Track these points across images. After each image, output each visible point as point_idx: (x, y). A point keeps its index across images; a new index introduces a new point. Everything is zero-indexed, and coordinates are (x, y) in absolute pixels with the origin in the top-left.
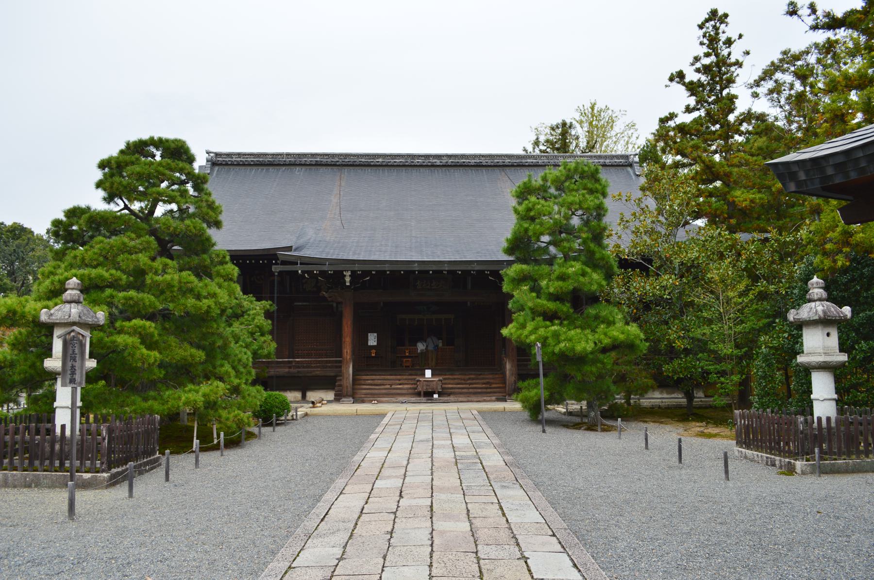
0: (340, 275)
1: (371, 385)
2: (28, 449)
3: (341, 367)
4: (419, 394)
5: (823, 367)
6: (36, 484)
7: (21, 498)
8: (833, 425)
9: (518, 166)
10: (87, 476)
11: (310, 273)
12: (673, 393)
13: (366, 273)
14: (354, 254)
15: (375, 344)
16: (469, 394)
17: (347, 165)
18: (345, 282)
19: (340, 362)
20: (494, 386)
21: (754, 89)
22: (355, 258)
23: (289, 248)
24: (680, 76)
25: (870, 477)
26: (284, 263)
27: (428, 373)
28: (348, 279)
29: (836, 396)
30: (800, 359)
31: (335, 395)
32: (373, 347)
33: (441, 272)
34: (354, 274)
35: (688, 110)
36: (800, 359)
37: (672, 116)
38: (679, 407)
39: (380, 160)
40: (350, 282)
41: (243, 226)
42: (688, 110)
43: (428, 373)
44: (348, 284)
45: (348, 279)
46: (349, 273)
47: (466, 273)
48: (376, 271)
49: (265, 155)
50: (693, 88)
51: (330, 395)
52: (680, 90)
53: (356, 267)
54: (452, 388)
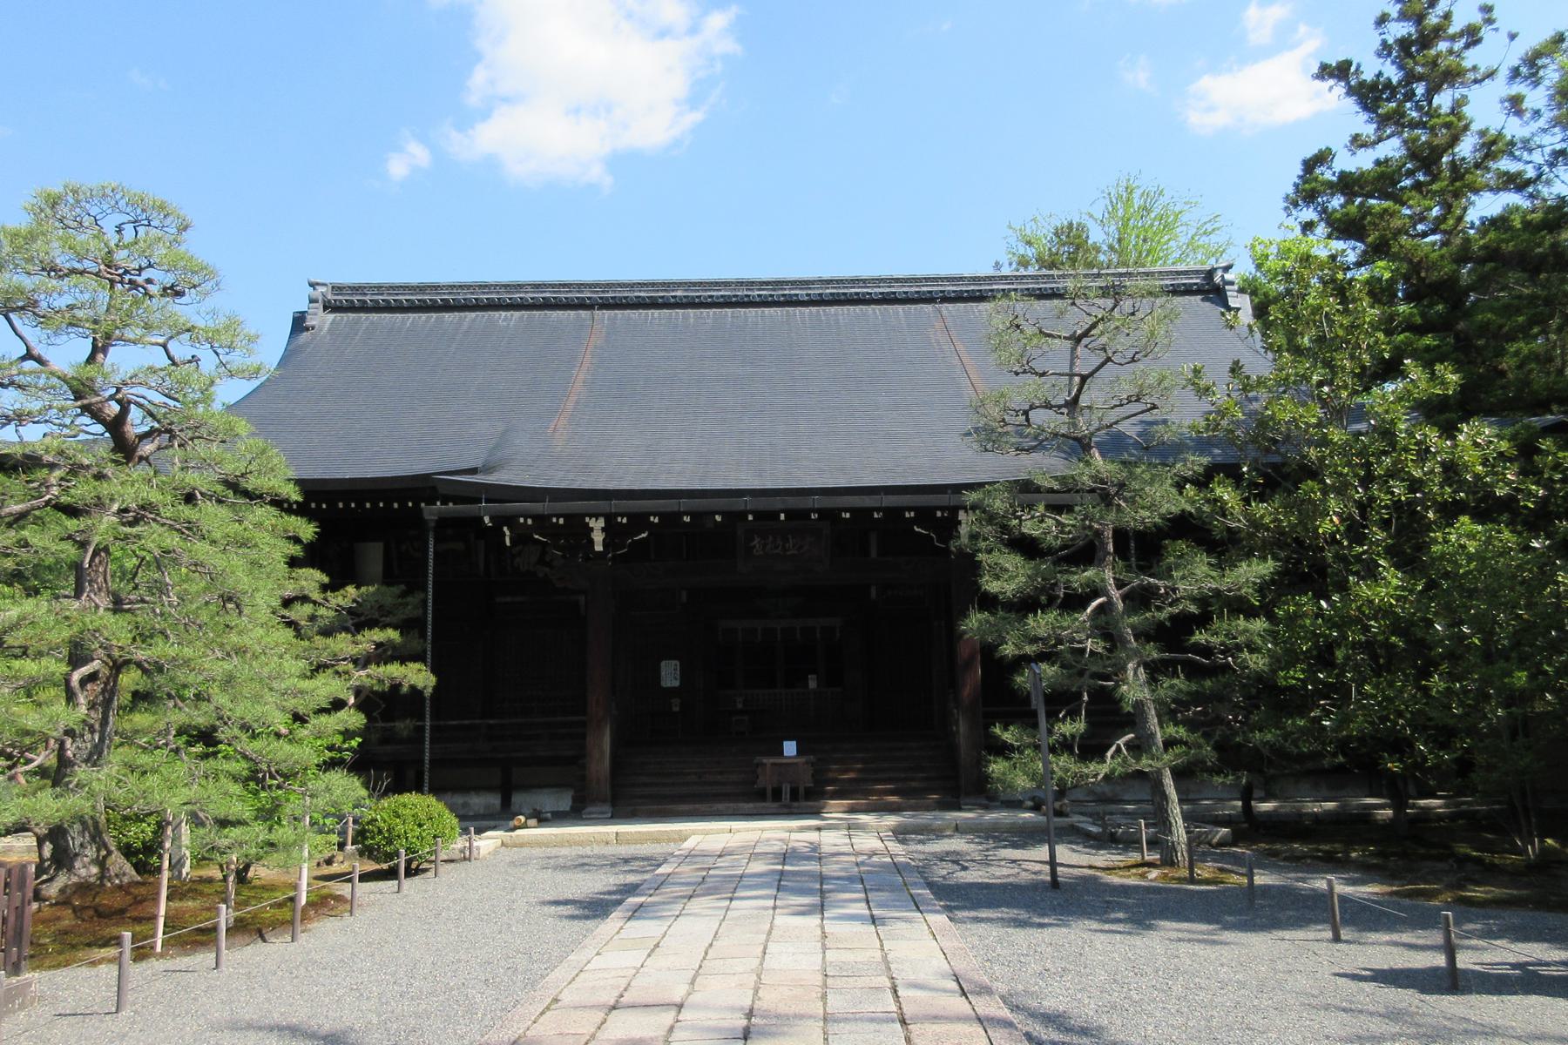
0: (577, 528)
3: (584, 737)
4: (761, 796)
11: (510, 520)
13: (639, 520)
14: (357, 322)
15: (677, 684)
18: (592, 542)
21: (1519, 88)
22: (611, 486)
24: (1341, 71)
25: (1561, 1003)
27: (790, 748)
28: (598, 538)
31: (574, 799)
32: (672, 690)
33: (803, 514)
35: (1358, 142)
37: (1322, 158)
38: (1434, 971)
39: (679, 293)
42: (1358, 142)
43: (790, 748)
44: (599, 548)
45: (598, 538)
46: (601, 523)
47: (861, 514)
48: (788, 513)
49: (435, 288)
50: (1369, 95)
52: (1334, 95)
53: (615, 505)
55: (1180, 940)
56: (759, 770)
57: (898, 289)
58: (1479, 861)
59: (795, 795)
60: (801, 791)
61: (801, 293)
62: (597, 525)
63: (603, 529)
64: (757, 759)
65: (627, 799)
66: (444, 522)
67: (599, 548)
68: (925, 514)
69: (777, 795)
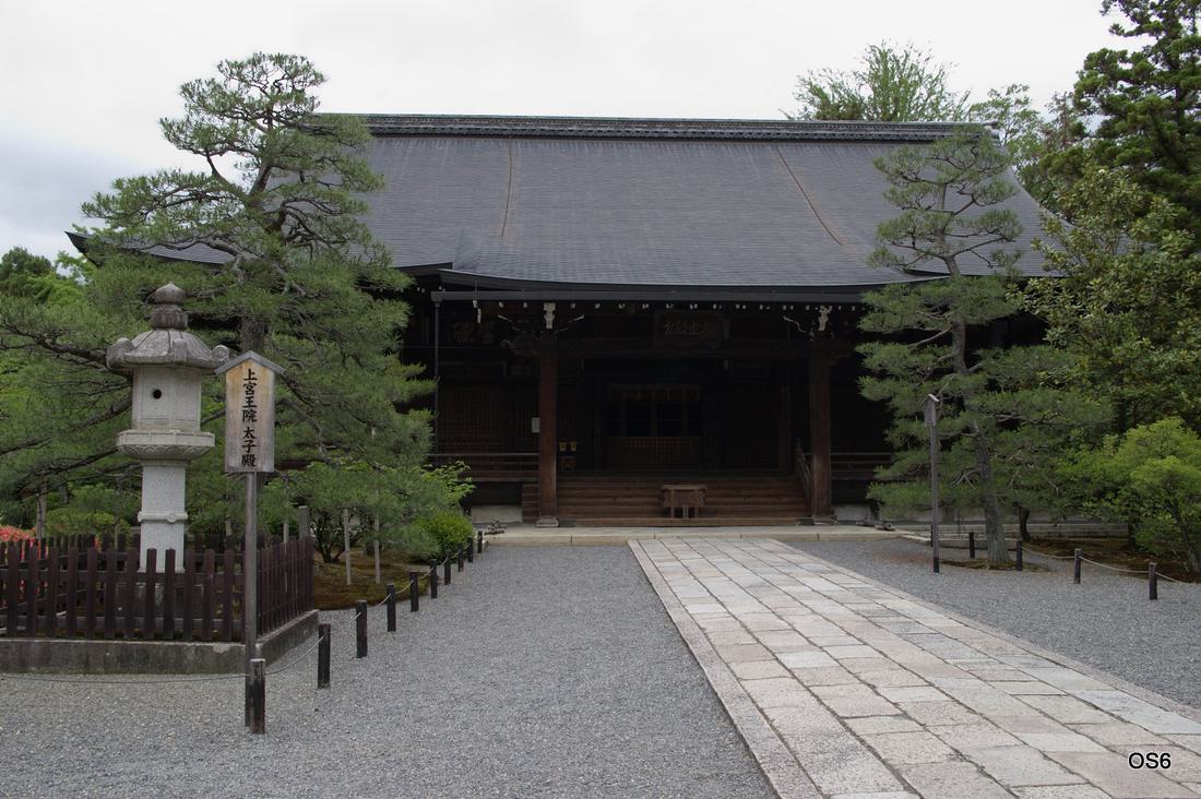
1: (583, 497)
2: (70, 600)
3: (537, 467)
4: (665, 513)
5: (170, 457)
6: (47, 663)
7: (121, 692)
8: (179, 567)
9: (802, 140)
10: (221, 647)
12: (790, 524)
13: (585, 306)
16: (613, 514)
17: (521, 136)
19: (537, 458)
20: (619, 500)
23: (449, 265)
26: (450, 287)
28: (549, 318)
29: (185, 516)
30: (126, 439)
33: (661, 304)
34: (562, 307)
36: (126, 439)
39: (575, 128)
40: (554, 323)
41: (412, 227)
44: (549, 326)
45: (549, 318)
48: (505, 302)
51: (515, 515)
54: (716, 503)
55: (95, 458)
56: (665, 495)
57: (745, 131)
58: (440, 457)
59: (691, 513)
60: (696, 511)
61: (670, 132)
62: (550, 308)
63: (554, 312)
64: (665, 486)
65: (837, 563)
66: (446, 304)
67: (549, 326)
68: (800, 306)
69: (679, 513)
